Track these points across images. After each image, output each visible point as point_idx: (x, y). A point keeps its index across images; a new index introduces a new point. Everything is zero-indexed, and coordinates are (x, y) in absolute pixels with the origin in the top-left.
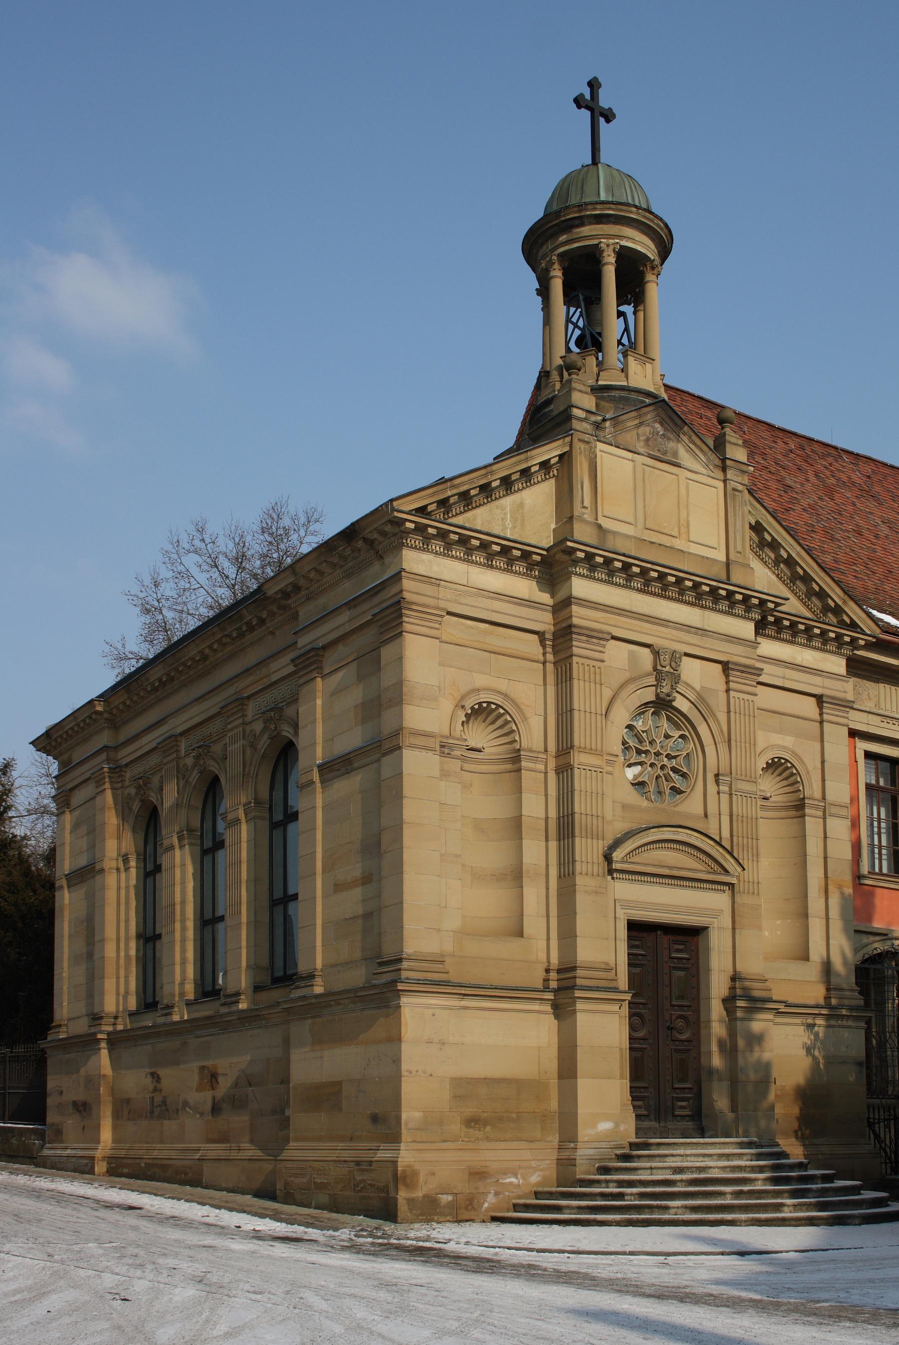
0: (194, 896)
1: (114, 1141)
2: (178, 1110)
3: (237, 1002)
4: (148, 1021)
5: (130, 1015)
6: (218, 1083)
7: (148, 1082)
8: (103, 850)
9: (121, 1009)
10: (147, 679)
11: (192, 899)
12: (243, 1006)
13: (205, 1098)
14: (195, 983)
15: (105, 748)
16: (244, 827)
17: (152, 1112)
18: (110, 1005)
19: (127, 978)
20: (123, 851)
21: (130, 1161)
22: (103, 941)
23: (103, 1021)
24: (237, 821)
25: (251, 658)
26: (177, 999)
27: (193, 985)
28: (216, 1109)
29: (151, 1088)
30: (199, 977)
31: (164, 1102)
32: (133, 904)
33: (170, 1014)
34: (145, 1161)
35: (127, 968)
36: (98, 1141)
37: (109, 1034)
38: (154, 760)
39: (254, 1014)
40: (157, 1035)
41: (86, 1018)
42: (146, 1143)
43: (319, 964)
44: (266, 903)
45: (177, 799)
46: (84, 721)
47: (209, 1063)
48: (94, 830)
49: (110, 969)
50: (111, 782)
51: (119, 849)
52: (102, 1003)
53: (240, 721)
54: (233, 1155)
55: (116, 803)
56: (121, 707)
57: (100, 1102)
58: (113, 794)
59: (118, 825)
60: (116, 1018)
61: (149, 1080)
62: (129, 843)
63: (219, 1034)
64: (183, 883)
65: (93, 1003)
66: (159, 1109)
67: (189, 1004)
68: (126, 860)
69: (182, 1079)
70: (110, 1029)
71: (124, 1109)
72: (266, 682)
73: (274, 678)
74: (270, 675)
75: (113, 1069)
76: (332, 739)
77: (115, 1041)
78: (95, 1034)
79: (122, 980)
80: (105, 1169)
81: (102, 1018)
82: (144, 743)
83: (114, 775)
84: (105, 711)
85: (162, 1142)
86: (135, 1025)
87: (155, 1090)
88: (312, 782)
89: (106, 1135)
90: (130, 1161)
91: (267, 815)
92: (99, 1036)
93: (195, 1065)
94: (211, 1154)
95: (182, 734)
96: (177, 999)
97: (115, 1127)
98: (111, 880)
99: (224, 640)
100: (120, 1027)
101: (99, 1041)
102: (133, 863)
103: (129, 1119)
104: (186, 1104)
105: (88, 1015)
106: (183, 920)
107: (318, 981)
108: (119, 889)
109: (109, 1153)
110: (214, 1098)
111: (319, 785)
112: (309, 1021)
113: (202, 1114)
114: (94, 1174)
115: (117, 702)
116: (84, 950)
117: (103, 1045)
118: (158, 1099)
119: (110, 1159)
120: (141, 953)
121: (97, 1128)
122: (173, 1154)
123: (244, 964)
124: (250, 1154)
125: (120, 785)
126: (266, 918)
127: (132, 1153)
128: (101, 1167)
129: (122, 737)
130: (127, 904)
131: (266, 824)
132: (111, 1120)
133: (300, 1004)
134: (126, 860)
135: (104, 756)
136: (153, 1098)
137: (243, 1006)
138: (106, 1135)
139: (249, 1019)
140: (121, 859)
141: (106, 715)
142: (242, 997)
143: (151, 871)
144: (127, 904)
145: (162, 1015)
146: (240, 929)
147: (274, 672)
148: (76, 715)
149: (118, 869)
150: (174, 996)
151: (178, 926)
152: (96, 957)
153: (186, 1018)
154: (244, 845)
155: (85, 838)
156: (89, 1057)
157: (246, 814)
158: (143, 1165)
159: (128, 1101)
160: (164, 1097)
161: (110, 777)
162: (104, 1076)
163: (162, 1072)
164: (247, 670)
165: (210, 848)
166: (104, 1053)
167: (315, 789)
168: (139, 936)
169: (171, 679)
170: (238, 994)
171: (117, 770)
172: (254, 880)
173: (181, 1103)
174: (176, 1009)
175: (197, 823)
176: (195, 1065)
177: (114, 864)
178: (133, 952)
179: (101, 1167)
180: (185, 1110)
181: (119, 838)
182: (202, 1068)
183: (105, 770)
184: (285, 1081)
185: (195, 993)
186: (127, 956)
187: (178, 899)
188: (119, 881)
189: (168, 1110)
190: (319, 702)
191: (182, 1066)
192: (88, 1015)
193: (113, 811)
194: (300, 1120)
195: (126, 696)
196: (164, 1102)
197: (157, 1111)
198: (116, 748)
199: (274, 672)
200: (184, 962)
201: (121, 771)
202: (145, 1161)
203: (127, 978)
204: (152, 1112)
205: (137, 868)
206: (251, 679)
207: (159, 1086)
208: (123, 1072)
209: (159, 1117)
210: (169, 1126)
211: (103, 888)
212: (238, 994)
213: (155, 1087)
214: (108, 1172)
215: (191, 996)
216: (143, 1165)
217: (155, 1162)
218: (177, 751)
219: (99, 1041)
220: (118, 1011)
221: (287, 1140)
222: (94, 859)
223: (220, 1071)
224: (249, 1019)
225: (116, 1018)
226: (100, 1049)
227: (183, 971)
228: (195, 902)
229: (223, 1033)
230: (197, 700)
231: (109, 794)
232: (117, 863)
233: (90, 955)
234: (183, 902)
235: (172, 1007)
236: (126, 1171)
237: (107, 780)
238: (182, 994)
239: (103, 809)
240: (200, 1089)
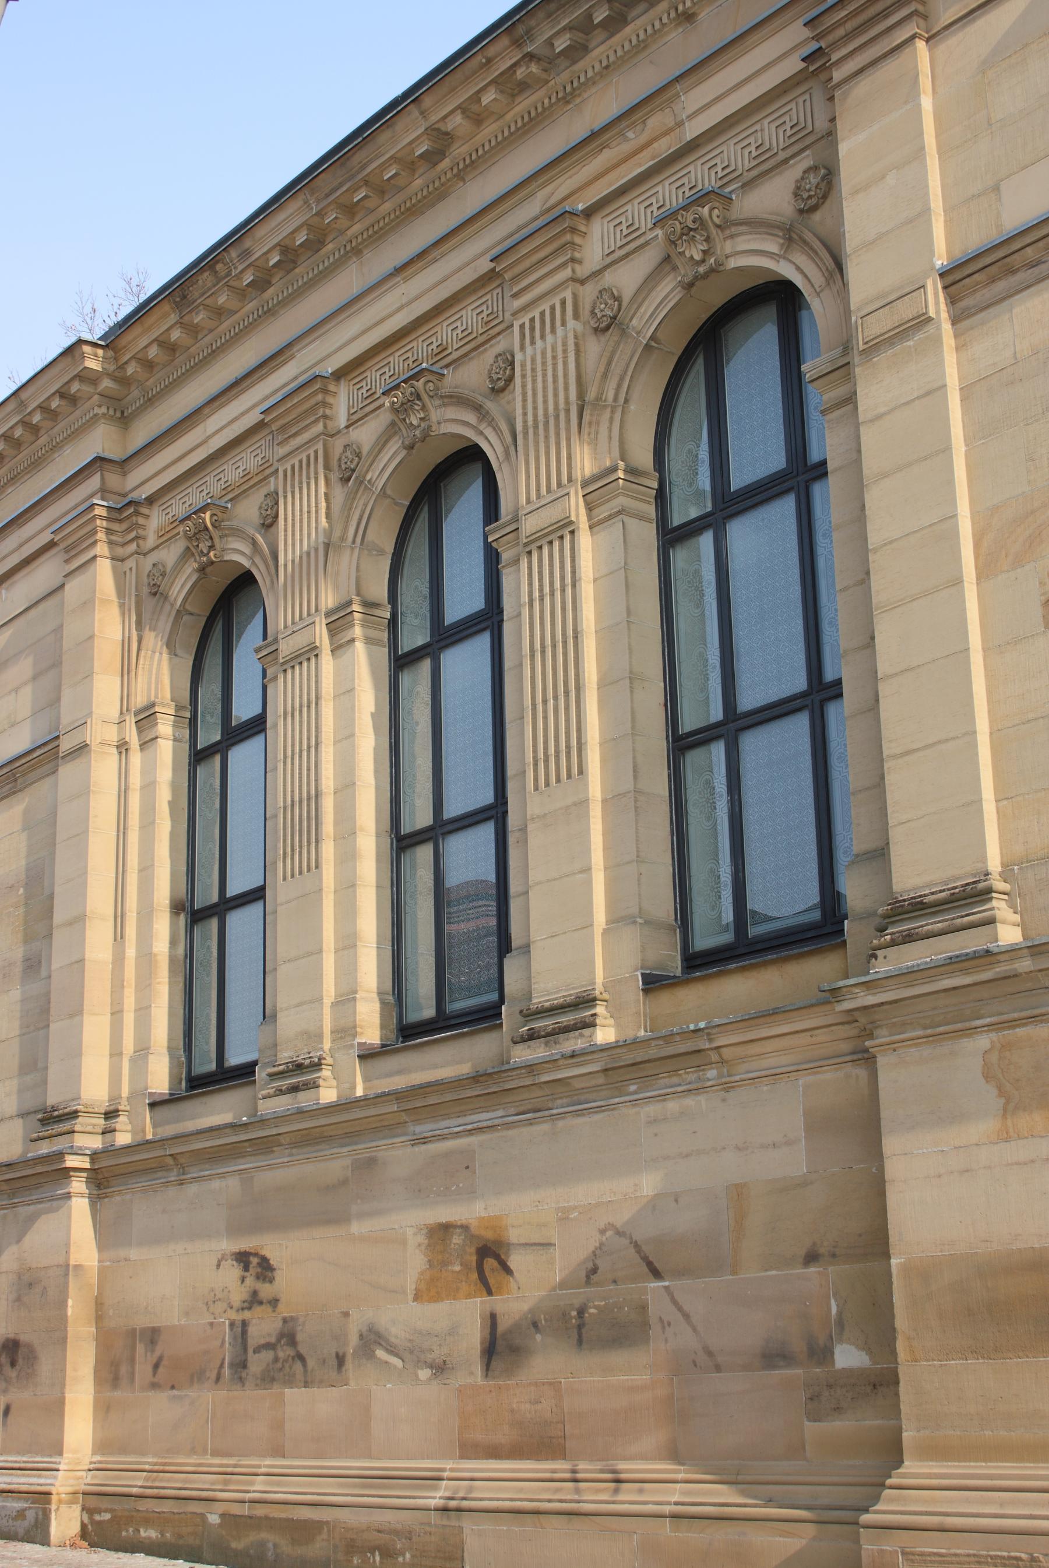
0: (376, 772)
1: (101, 1446)
2: (341, 1360)
3: (590, 1024)
4: (219, 1110)
5: (153, 1105)
6: (508, 1271)
7: (231, 1281)
8: (87, 700)
9: (125, 1092)
10: (246, 253)
11: (372, 781)
12: (605, 1034)
13: (464, 1317)
14: (383, 1003)
15: (99, 462)
16: (585, 540)
17: (241, 1365)
18: (94, 1086)
19: (143, 1011)
20: (139, 700)
21: (166, 1507)
22: (79, 920)
23: (80, 1124)
24: (565, 528)
25: (602, 106)
26: (327, 1045)
27: (377, 1006)
28: (499, 1348)
29: (238, 1294)
30: (388, 985)
31: (288, 1336)
32: (164, 826)
33: (314, 1085)
34: (221, 1508)
35: (144, 985)
36: (58, 1449)
37: (94, 1156)
38: (248, 460)
39: (682, 1048)
40: (265, 1146)
41: (19, 1123)
42: (215, 1453)
43: (994, 863)
44: (657, 743)
45: (329, 534)
46: (43, 408)
47: (470, 1212)
48: (57, 664)
49: (97, 991)
50: (111, 543)
51: (125, 698)
52: (74, 1076)
53: (567, 273)
54: (595, 1497)
55: (121, 592)
56: (153, 352)
57: (63, 1341)
58: (115, 569)
59: (126, 644)
60: (110, 1115)
61: (232, 1272)
62: (161, 676)
63: (508, 1126)
64: (346, 737)
65: (45, 1082)
66: (267, 1356)
67: (367, 1055)
68: (146, 718)
69: (372, 1263)
70: (96, 1143)
71: (135, 1356)
72: (665, 147)
73: (692, 130)
74: (680, 124)
75: (101, 1247)
76: (996, 188)
77: (104, 1177)
78: (60, 1155)
79: (129, 1019)
80: (75, 1528)
81: (74, 1115)
82: (211, 430)
83: (116, 527)
84: (105, 373)
85: (279, 1452)
86: (170, 1130)
87: (254, 1300)
88: (923, 321)
89: (79, 1429)
90: (166, 1507)
91: (651, 510)
92: (71, 1161)
93: (411, 1221)
94: (487, 1495)
95: (339, 375)
96: (327, 1045)
97: (103, 1409)
98: (104, 769)
99: (520, 73)
100: (123, 1138)
101: (66, 1173)
102: (165, 727)
103: (154, 1386)
104: (372, 1339)
105: (23, 1115)
106: (347, 834)
107: (999, 906)
108: (123, 794)
109: (87, 1480)
110: (493, 1319)
111: (946, 327)
112: (984, 1041)
113: (440, 1369)
114: (45, 1542)
115: (143, 342)
116: (19, 953)
117: (78, 1185)
118: (264, 1326)
119: (92, 1500)
120: (181, 950)
121: (56, 1409)
122: (331, 1490)
123: (600, 917)
124: (672, 1496)
125: (133, 547)
126: (660, 786)
127: (171, 1484)
128: (65, 1522)
129: (143, 432)
130: (148, 825)
131: (647, 534)
132: (92, 1390)
133: (947, 983)
134: (146, 718)
135: (94, 482)
136: (244, 1324)
137: (605, 1034)
138: (79, 1429)
139: (630, 1070)
140: (131, 721)
141: (106, 383)
142: (600, 1009)
143: (219, 738)
144: (148, 825)
145: (280, 1092)
146: (586, 816)
147: (691, 117)
148: (24, 395)
149: (123, 747)
150: (320, 1036)
151: (328, 850)
152: (58, 961)
153: (359, 1092)
154: (587, 591)
155: (28, 690)
156: (32, 1219)
157: (590, 509)
158: (214, 1519)
159: (152, 1336)
160: (285, 1321)
161: (109, 531)
162: (77, 1267)
163: (274, 1247)
164: (594, 135)
165: (443, 630)
166: (80, 1207)
167: (937, 340)
168: (177, 907)
169: (314, 245)
170: (587, 1001)
171: (127, 511)
172: (618, 681)
173: (353, 1340)
174: (326, 1072)
175: (380, 591)
176: (411, 1221)
177: (112, 734)
178: (161, 946)
179: (65, 1522)
180: (371, 1356)
181: (127, 671)
182: (441, 1232)
183: (98, 511)
184: (876, 1243)
185: (383, 1027)
186: (146, 957)
187: (328, 781)
188: (124, 774)
189: (301, 1358)
190: (927, 103)
191: (356, 1228)
192: (23, 1115)
193: (115, 611)
194: (936, 1382)
195: (173, 318)
196: (288, 1336)
197: (257, 1363)
198: (124, 465)
199: (691, 117)
200: (348, 944)
201: (137, 513)
202: (221, 1508)
203: (143, 1011)
204: (241, 1365)
205: (175, 740)
206: (606, 157)
207: (266, 1290)
208: (134, 1254)
209: (268, 1379)
210: (305, 1405)
211: (84, 792)
212: (587, 1001)
213: (255, 1293)
214: (84, 1534)
215: (372, 1035)
216: (214, 1519)
217: (260, 1511)
218: (325, 417)
219: (66, 1173)
220: (114, 1098)
221: (892, 1452)
222: (57, 729)
223: (514, 1236)
224: (630, 1070)
225: (110, 1115)
226: (68, 1196)
227: (348, 969)
228: (378, 788)
229: (530, 1123)
230: (399, 270)
231: (104, 571)
232: (121, 731)
233: (33, 966)
234: (347, 787)
235: (317, 1066)
236: (149, 1534)
237: (101, 535)
238: (345, 1032)
239: (88, 604)
240: (430, 1290)
